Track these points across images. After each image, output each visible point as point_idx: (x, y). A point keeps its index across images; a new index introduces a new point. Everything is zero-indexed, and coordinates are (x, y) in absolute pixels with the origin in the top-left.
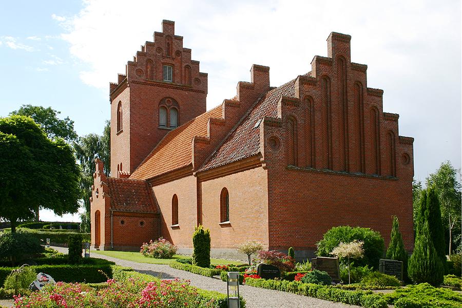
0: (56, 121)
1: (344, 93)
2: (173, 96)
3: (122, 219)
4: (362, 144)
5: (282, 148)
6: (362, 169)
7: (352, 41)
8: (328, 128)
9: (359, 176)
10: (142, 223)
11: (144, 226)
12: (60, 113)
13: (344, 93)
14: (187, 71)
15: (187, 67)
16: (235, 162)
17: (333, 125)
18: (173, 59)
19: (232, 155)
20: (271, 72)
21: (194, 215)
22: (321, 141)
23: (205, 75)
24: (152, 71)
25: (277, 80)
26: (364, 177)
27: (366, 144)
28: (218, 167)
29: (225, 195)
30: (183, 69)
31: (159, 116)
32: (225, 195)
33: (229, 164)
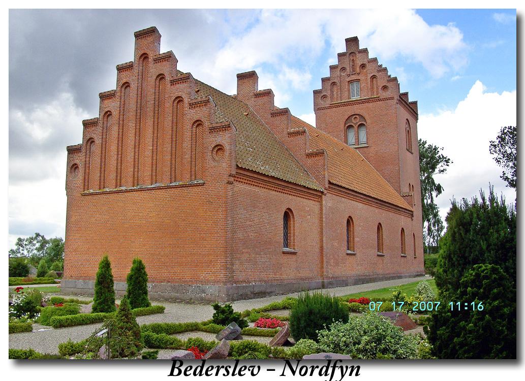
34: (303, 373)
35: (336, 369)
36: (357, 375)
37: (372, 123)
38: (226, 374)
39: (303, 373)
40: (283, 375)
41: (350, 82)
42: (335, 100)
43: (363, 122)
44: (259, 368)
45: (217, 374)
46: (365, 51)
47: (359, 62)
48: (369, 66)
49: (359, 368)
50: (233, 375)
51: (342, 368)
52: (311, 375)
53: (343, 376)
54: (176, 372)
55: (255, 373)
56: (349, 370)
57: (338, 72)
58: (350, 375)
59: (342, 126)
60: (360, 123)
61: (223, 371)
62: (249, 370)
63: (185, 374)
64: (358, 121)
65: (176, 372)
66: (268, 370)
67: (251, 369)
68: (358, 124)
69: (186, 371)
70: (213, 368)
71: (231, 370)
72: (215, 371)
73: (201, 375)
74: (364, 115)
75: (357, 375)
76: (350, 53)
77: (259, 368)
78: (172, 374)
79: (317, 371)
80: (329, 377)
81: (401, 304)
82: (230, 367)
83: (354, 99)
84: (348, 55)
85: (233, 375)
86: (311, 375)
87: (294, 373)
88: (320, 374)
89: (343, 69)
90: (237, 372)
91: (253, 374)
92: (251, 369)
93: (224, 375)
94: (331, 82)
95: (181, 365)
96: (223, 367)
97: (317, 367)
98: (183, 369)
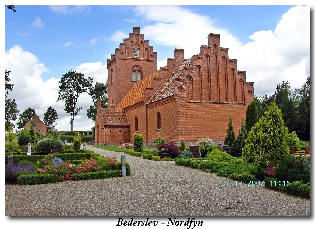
0: (278, 91)
1: (217, 63)
2: (139, 64)
3: (110, 129)
4: (227, 87)
5: (185, 92)
6: (227, 99)
7: (220, 37)
8: (209, 80)
9: (225, 103)
10: (120, 131)
11: (111, 132)
12: (11, 72)
13: (217, 63)
14: (146, 51)
15: (147, 49)
16: (163, 99)
17: (211, 79)
18: (139, 46)
19: (162, 96)
20: (229, 51)
21: (145, 126)
22: (205, 87)
23: (156, 53)
24: (128, 52)
25: (188, 56)
26: (228, 104)
27: (228, 87)
28: (155, 102)
29: (159, 115)
30: (144, 50)
31: (131, 75)
32: (159, 115)
33: (160, 100)
34: (177, 224)
35: (192, 222)
36: (201, 225)
37: (145, 71)
38: (143, 225)
39: (177, 224)
40: (168, 225)
41: (135, 49)
42: (127, 56)
43: (140, 70)
44: (157, 222)
45: (138, 225)
46: (143, 35)
47: (140, 40)
48: (145, 43)
49: (202, 222)
50: (146, 225)
51: (194, 222)
52: (181, 225)
53: (195, 226)
54: (120, 224)
55: (156, 224)
56: (198, 223)
57: (129, 42)
58: (198, 225)
59: (130, 70)
60: (139, 70)
61: (141, 223)
62: (153, 223)
63: (124, 225)
64: (138, 69)
65: (120, 224)
66: (161, 223)
67: (154, 222)
68: (138, 70)
69: (124, 223)
70: (136, 222)
71: (145, 223)
72: (137, 223)
73: (131, 225)
74: (142, 68)
75: (201, 225)
76: (136, 35)
77: (157, 222)
78: (118, 225)
79: (183, 224)
80: (189, 226)
81: (241, 182)
82: (144, 222)
83: (135, 57)
84: (135, 35)
85: (146, 225)
86: (181, 225)
87: (173, 224)
88: (185, 225)
89: (132, 41)
90: (147, 224)
91: (155, 225)
92: (154, 222)
93: (142, 225)
94: (125, 46)
95: (122, 221)
96: (141, 222)
97: (183, 222)
98: (123, 222)
